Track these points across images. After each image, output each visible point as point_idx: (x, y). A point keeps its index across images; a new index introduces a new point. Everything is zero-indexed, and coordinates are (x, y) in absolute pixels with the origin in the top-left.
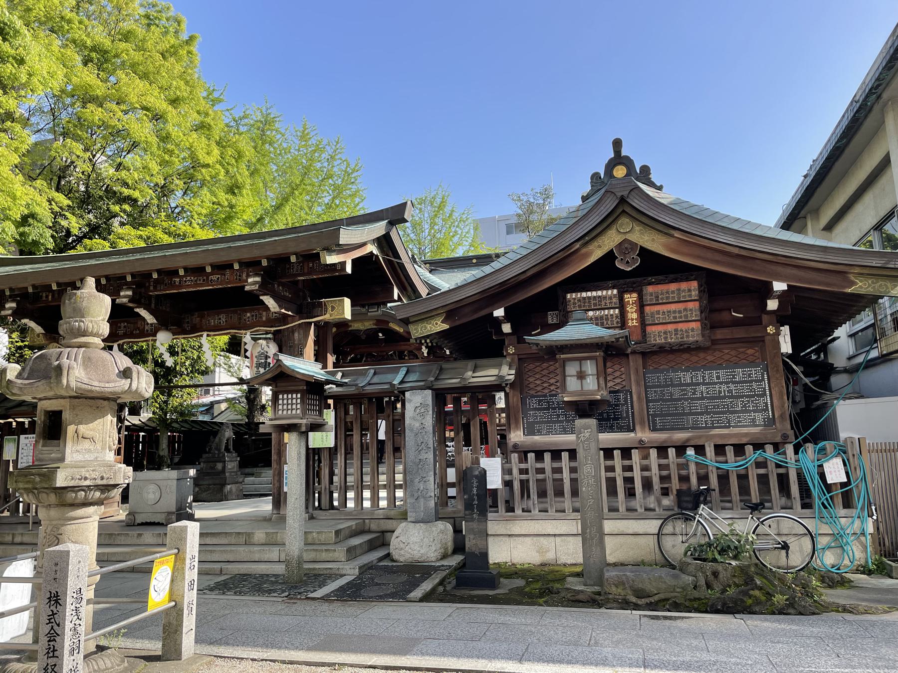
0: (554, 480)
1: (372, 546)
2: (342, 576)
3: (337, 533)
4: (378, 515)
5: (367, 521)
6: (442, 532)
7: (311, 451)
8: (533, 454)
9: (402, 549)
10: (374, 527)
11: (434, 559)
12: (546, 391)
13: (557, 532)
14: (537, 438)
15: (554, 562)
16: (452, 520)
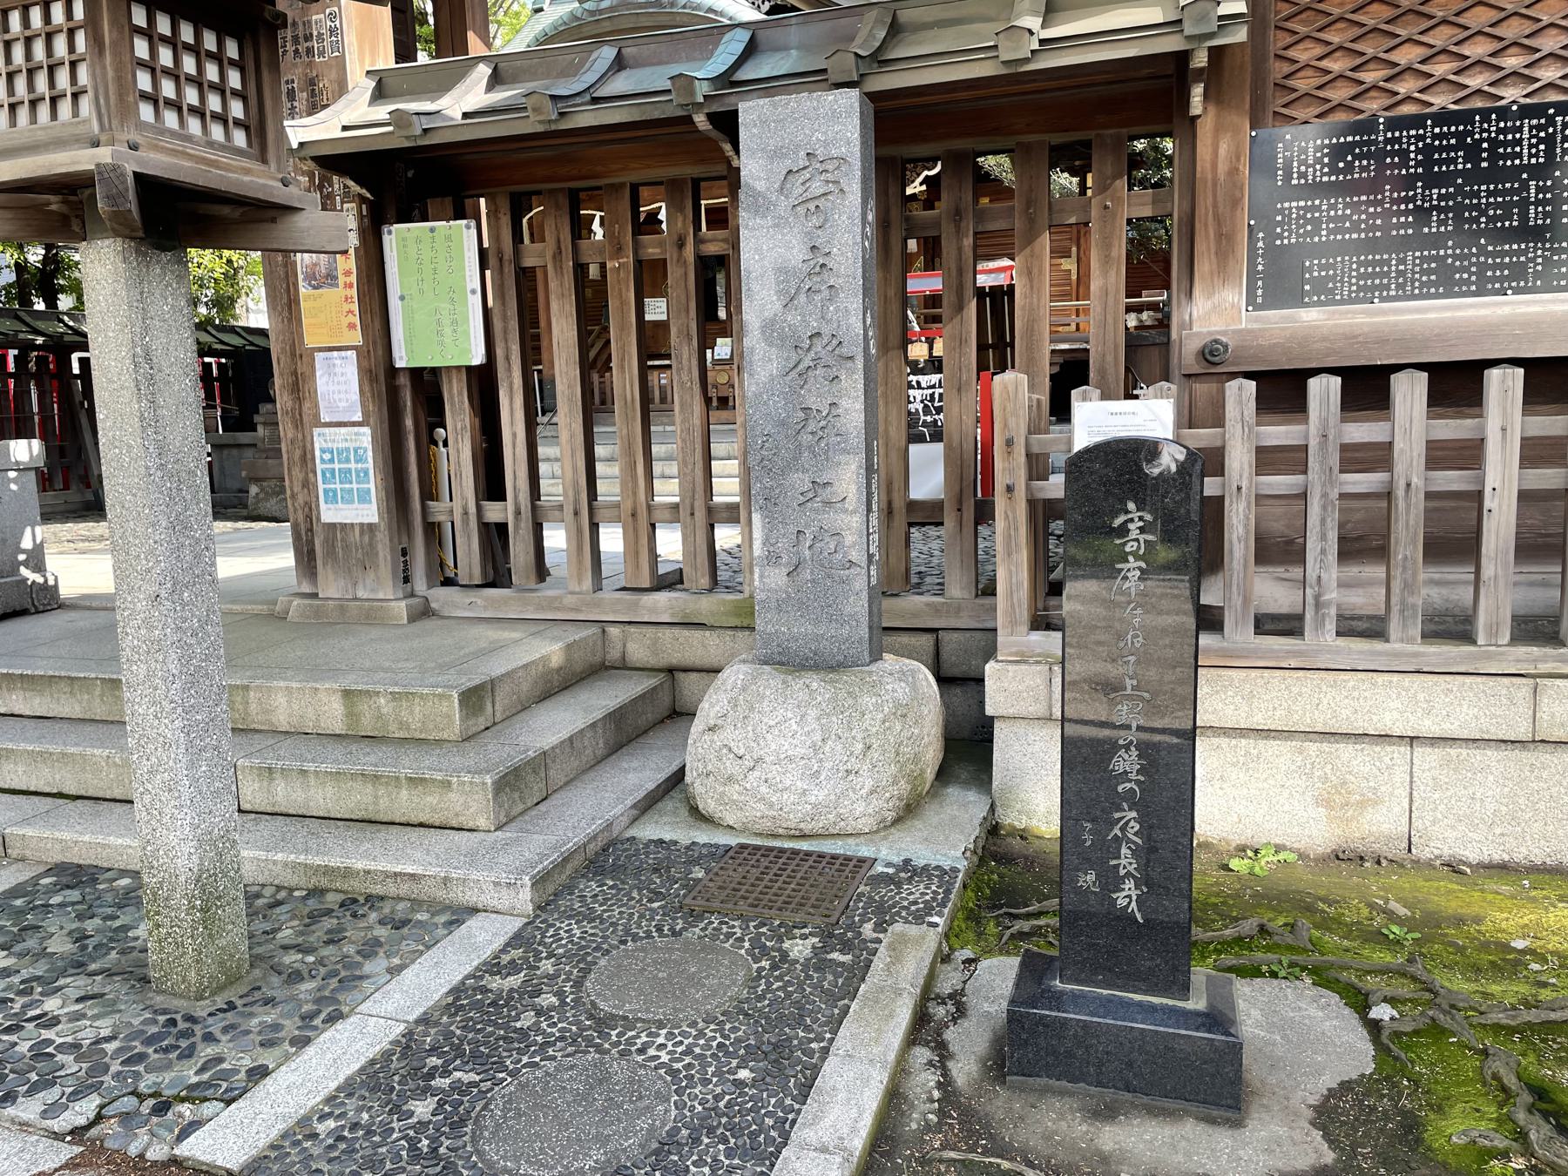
0: (1260, 498)
1: (622, 734)
2: (461, 914)
3: (473, 699)
4: (653, 610)
5: (614, 631)
6: (902, 713)
7: (404, 381)
8: (1251, 386)
9: (730, 779)
10: (639, 649)
11: (866, 824)
12: (1372, 105)
13: (1428, 727)
14: (1311, 317)
15: (1397, 850)
16: (926, 641)
